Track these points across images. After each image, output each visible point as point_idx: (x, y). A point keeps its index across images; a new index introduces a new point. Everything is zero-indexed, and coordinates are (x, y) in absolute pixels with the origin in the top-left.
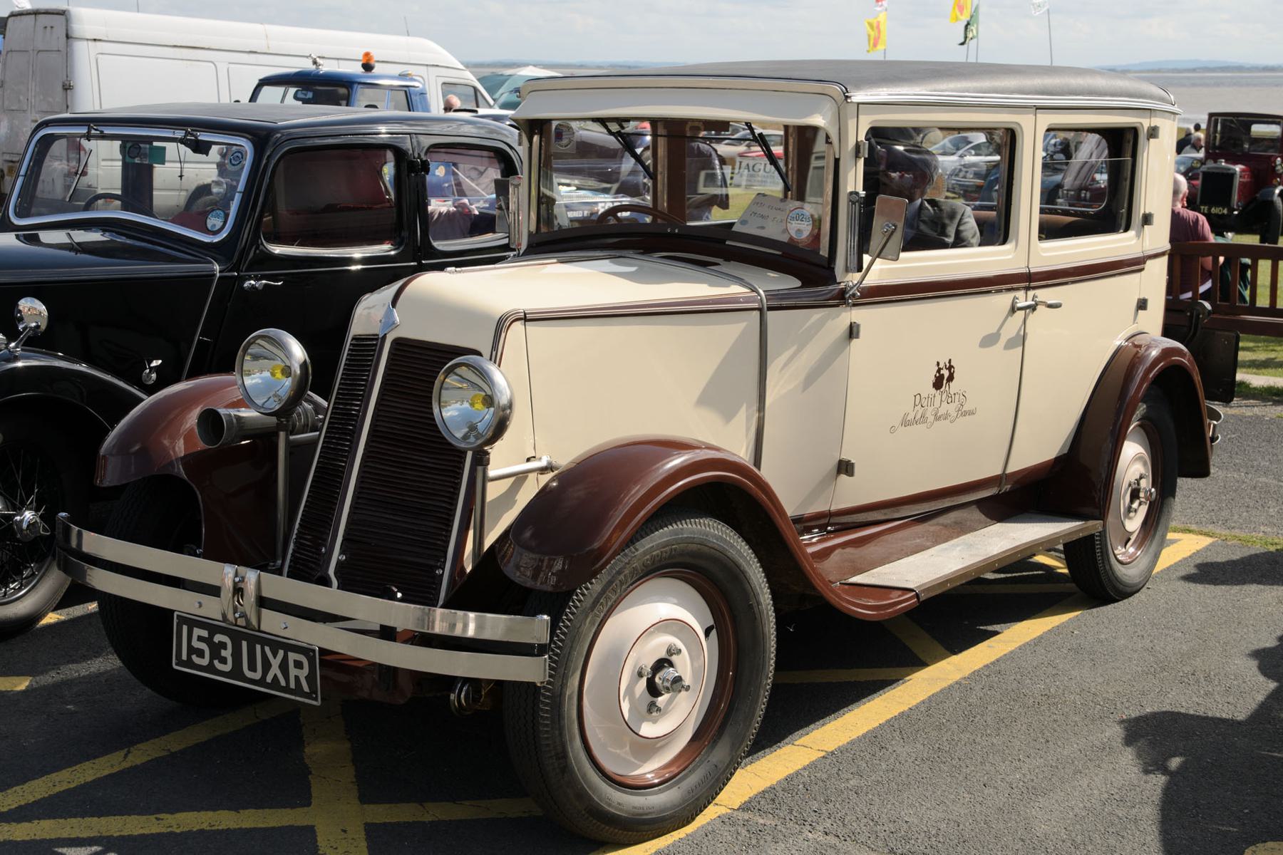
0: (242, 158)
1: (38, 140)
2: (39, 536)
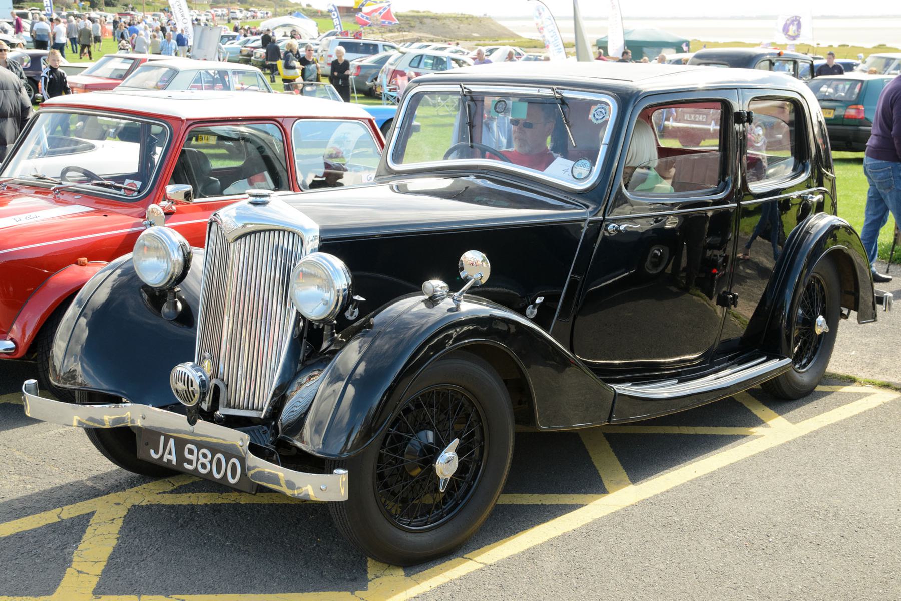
0: (606, 113)
1: (413, 96)
2: (6, 333)
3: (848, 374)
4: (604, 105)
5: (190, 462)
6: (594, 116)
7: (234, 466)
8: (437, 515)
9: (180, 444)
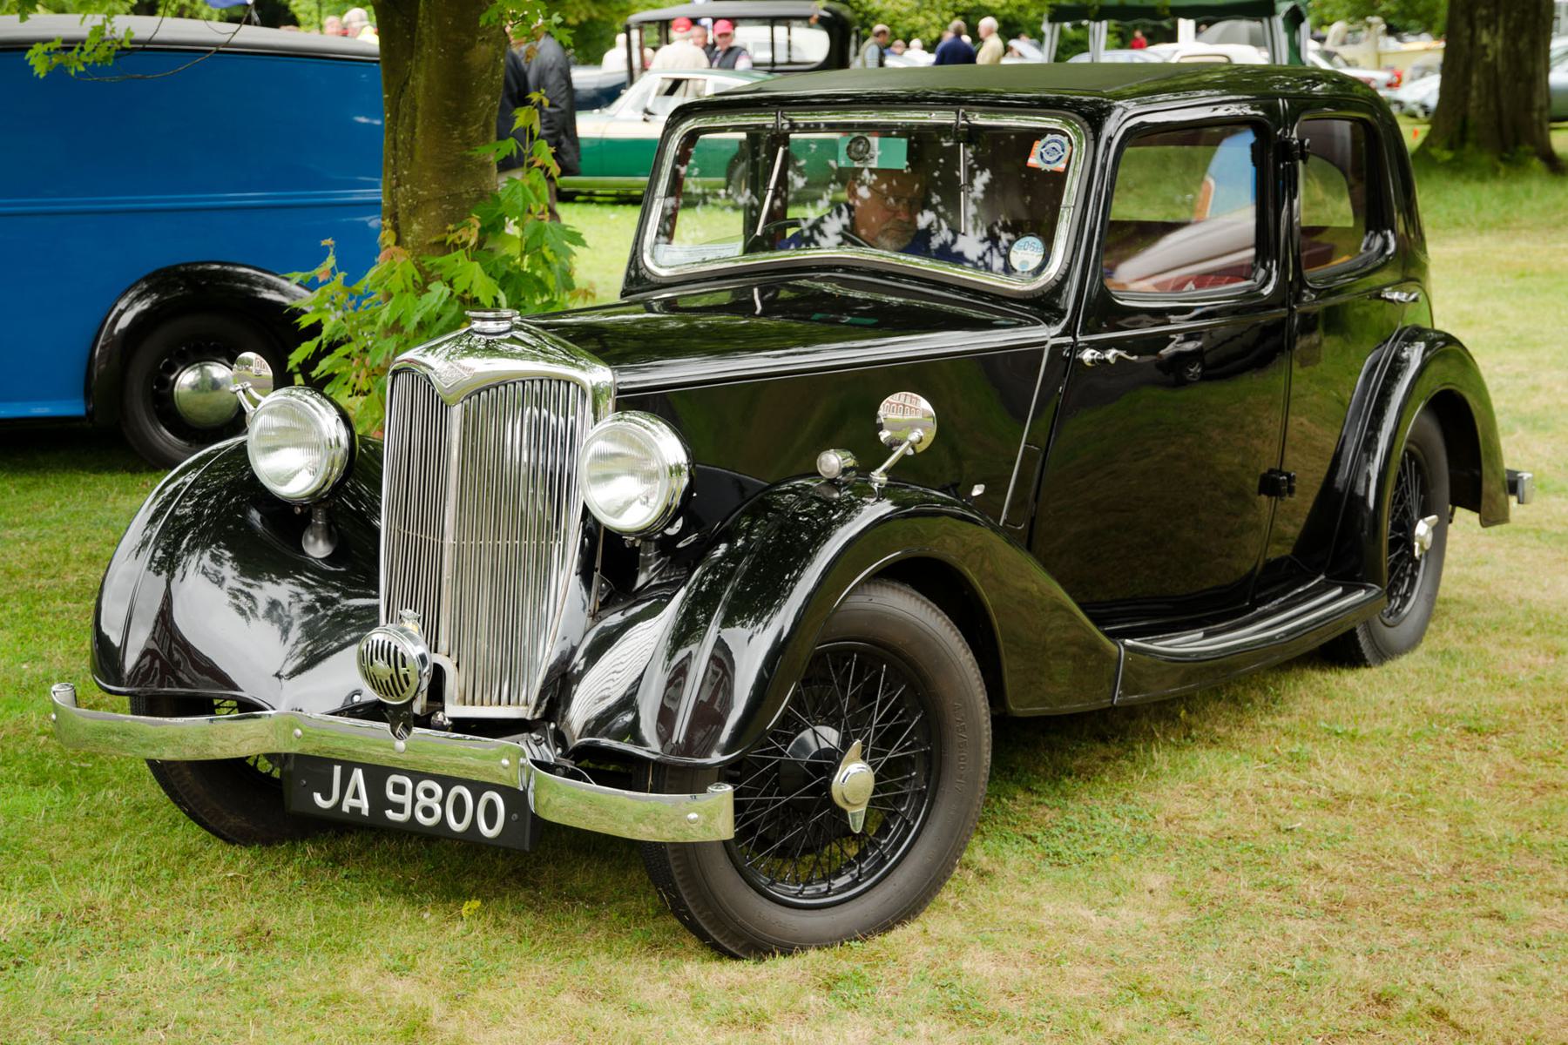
3: (762, 967)
4: (1058, 137)
5: (399, 808)
6: (1042, 157)
7: (491, 805)
8: (875, 857)
9: (377, 775)
